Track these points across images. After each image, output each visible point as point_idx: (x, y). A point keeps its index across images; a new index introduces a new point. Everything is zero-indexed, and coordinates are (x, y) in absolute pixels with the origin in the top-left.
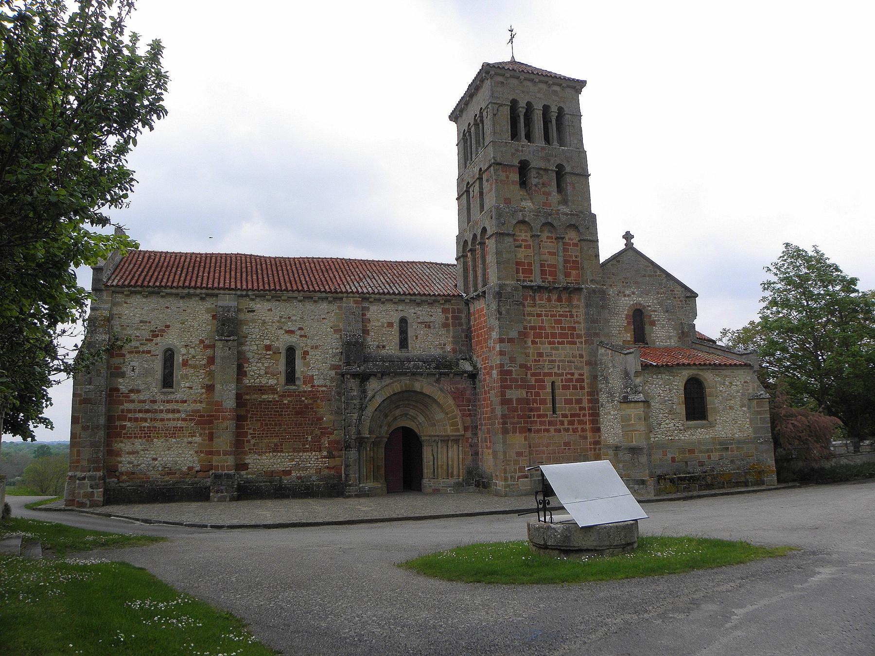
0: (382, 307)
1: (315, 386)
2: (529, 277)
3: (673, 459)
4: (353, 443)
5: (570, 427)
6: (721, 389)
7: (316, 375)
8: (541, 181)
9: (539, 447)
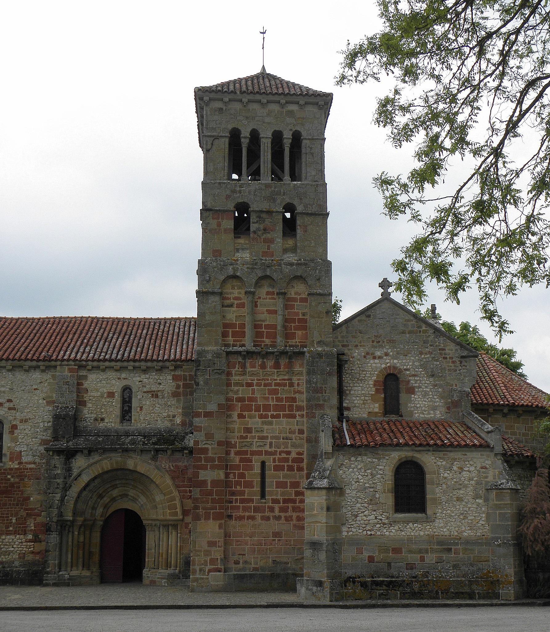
0: (102, 376)
2: (241, 341)
3: (371, 559)
5: (283, 514)
6: (446, 475)
8: (262, 226)
9: (241, 537)
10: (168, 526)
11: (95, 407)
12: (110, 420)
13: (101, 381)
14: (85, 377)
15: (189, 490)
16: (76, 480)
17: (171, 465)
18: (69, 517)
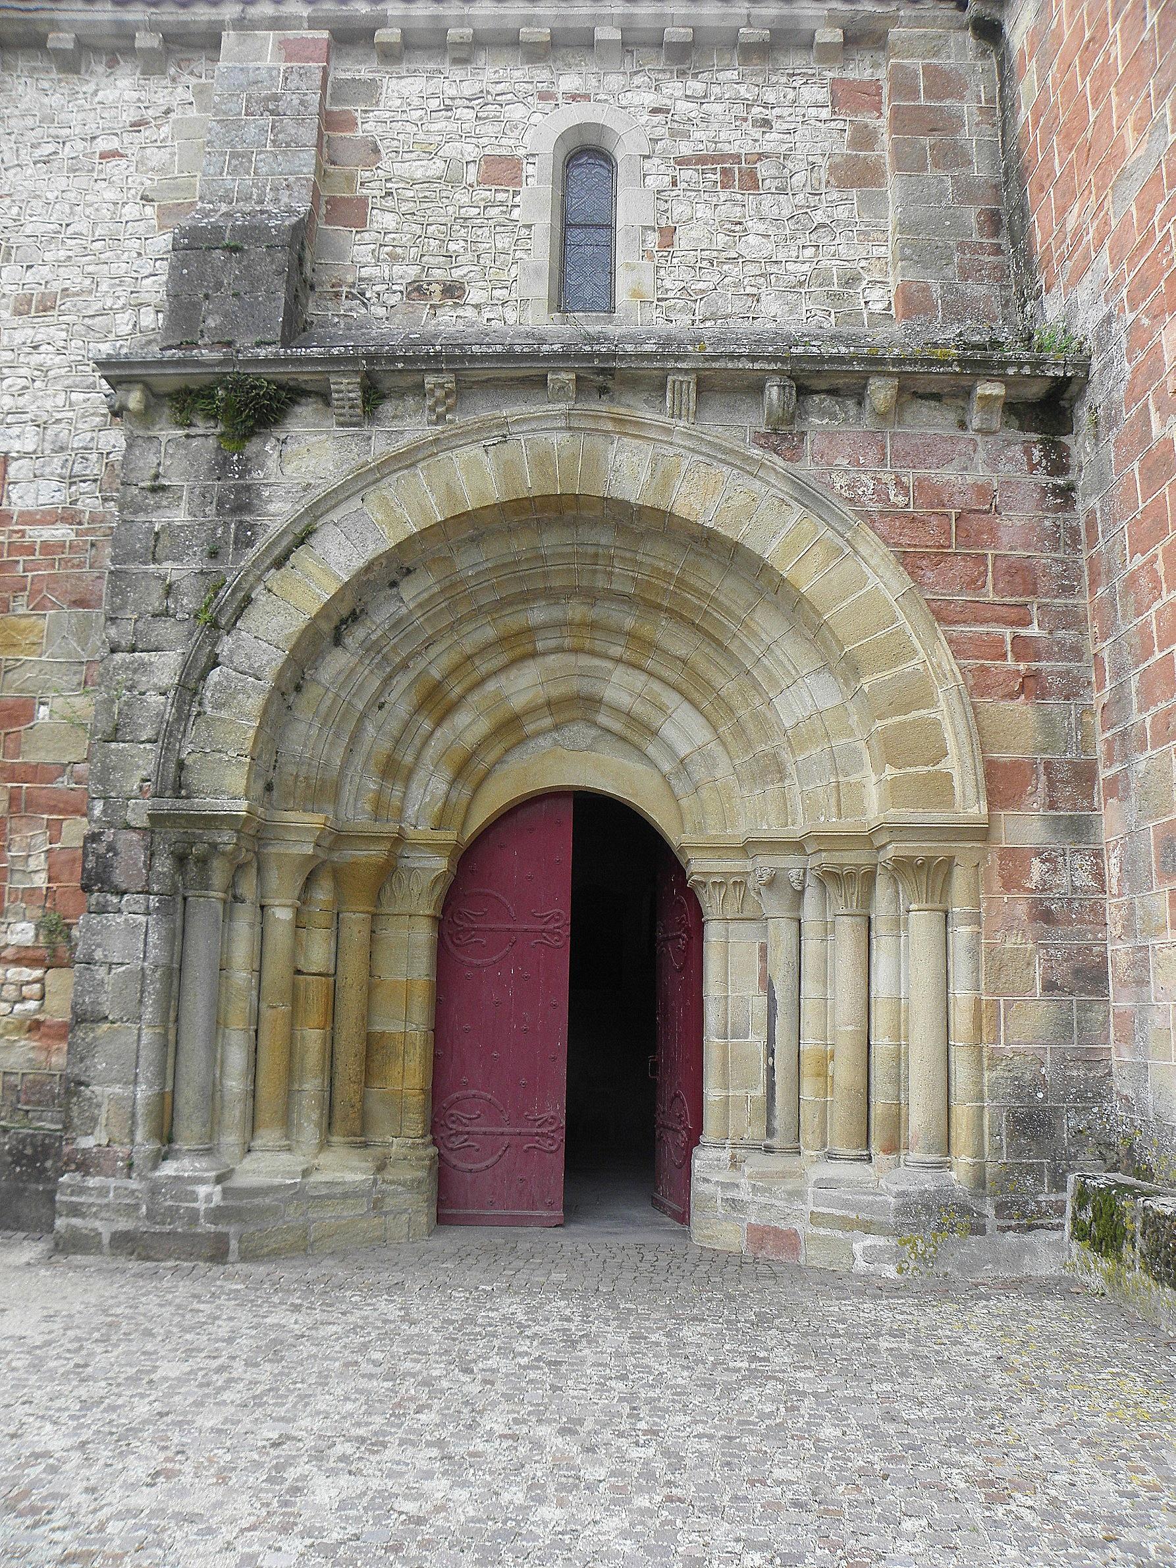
7: (26, 455)
10: (870, 878)
11: (417, 229)
12: (497, 293)
13: (448, 108)
14: (369, 91)
15: (1016, 638)
16: (279, 563)
17: (888, 478)
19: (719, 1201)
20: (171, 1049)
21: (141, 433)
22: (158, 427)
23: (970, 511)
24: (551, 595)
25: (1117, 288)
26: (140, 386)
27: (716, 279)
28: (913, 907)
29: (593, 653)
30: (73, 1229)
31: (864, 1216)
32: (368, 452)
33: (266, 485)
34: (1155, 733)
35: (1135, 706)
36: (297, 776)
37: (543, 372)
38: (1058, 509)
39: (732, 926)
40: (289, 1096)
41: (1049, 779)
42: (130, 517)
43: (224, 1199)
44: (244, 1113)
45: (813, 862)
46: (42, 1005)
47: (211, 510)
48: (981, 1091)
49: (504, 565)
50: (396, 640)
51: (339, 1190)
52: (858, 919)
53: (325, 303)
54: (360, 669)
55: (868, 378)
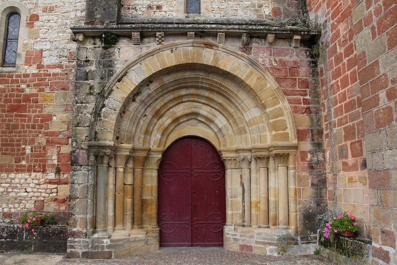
1: (43, 66)
4: (82, 155)
15: (304, 99)
16: (119, 81)
17: (272, 59)
18: (109, 140)
19: (232, 239)
20: (95, 205)
21: (82, 46)
22: (86, 45)
23: (292, 67)
24: (187, 87)
25: (328, 14)
26: (82, 34)
27: (227, 5)
28: (279, 165)
29: (197, 102)
30: (71, 251)
31: (269, 241)
32: (142, 52)
33: (116, 60)
34: (338, 123)
35: (333, 116)
36: (124, 135)
37: (187, 32)
38: (313, 67)
39: (233, 170)
40: (124, 215)
41: (312, 134)
42: (79, 68)
43: (110, 242)
44: (113, 221)
45: (254, 154)
46: (57, 194)
47: (101, 67)
48: (297, 210)
49: (176, 80)
50: (148, 99)
51: (137, 239)
52: (265, 168)
53: (126, 10)
54: (139, 107)
55: (267, 34)
